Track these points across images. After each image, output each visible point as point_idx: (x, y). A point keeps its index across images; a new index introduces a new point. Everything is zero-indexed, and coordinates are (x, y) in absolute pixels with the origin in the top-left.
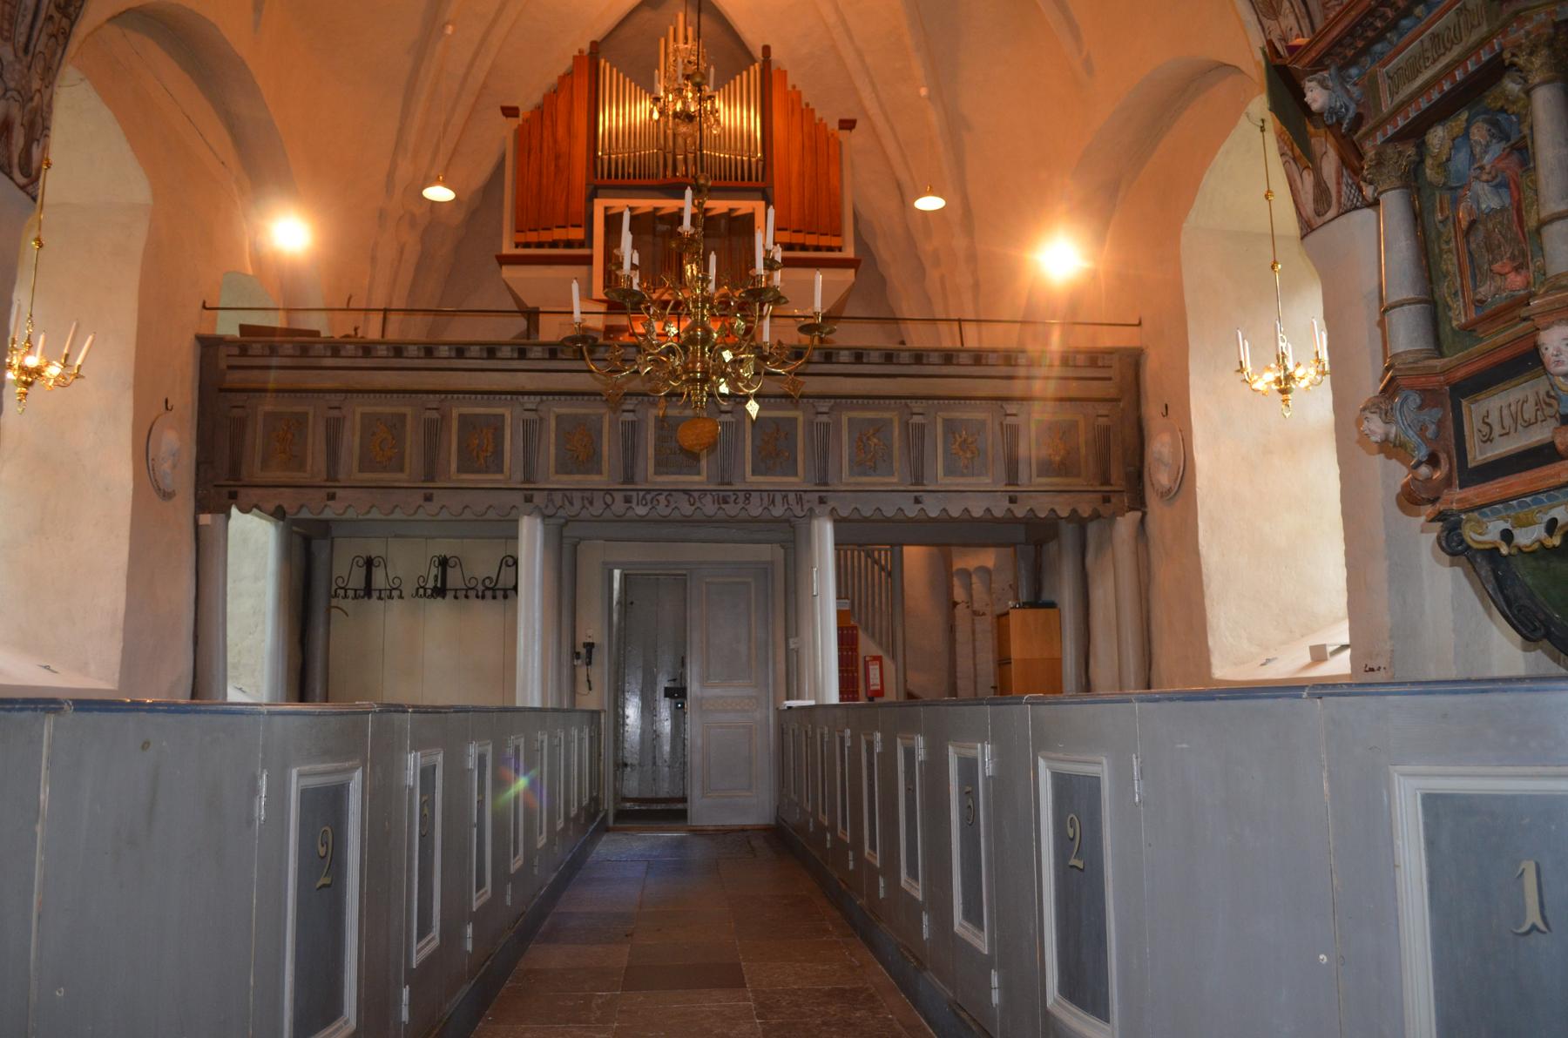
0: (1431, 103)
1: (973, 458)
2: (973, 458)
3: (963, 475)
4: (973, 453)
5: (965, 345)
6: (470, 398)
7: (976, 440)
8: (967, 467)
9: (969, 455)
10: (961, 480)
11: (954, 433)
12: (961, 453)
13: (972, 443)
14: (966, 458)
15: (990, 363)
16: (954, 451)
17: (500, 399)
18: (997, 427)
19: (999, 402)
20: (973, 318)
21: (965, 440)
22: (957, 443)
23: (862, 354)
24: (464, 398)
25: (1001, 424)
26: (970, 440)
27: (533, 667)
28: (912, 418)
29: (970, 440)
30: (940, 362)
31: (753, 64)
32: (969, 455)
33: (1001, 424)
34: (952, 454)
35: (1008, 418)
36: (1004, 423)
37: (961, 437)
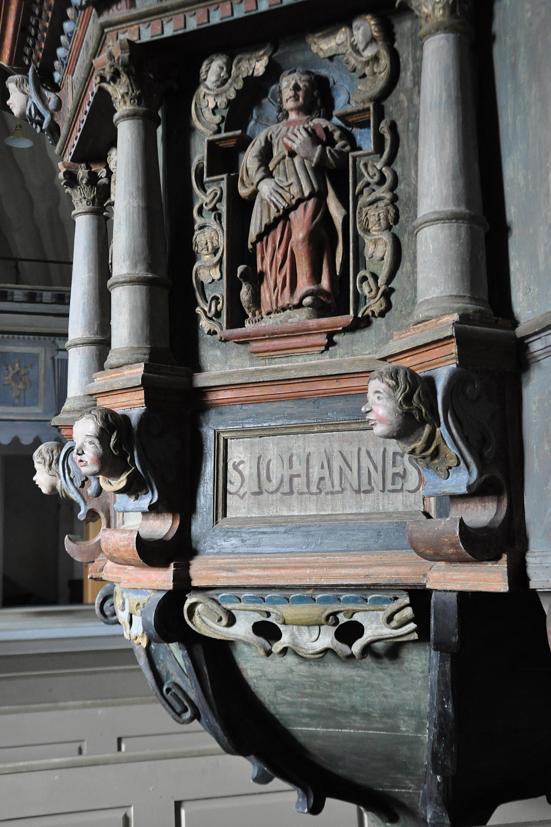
0: (91, 104)
1: (24, 390)
2: (24, 390)
3: (14, 405)
4: (25, 384)
5: (449, 333)
6: (13, 338)
7: (28, 372)
8: (18, 397)
9: (21, 386)
10: (25, 410)
11: (7, 365)
12: (13, 385)
13: (25, 375)
14: (18, 389)
15: (44, 301)
16: (6, 383)
17: (19, 338)
18: (50, 362)
19: (52, 338)
20: (54, 260)
21: (18, 373)
22: (10, 375)
23: (35, 294)
24: (8, 337)
25: (53, 359)
26: (23, 372)
27: (335, 566)
28: (58, 353)
29: (23, 372)
30: (25, 300)
31: (248, 76)
32: (21, 386)
33: (53, 359)
34: (4, 385)
35: (60, 353)
36: (56, 357)
37: (13, 369)
